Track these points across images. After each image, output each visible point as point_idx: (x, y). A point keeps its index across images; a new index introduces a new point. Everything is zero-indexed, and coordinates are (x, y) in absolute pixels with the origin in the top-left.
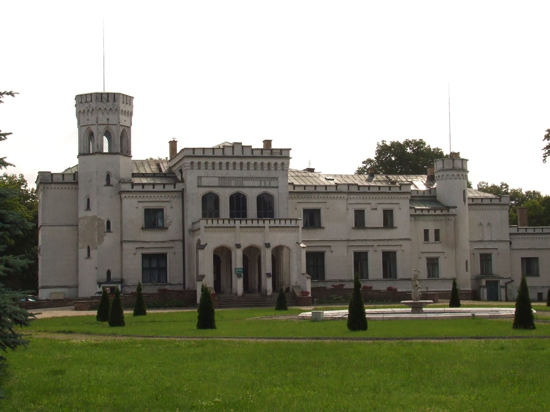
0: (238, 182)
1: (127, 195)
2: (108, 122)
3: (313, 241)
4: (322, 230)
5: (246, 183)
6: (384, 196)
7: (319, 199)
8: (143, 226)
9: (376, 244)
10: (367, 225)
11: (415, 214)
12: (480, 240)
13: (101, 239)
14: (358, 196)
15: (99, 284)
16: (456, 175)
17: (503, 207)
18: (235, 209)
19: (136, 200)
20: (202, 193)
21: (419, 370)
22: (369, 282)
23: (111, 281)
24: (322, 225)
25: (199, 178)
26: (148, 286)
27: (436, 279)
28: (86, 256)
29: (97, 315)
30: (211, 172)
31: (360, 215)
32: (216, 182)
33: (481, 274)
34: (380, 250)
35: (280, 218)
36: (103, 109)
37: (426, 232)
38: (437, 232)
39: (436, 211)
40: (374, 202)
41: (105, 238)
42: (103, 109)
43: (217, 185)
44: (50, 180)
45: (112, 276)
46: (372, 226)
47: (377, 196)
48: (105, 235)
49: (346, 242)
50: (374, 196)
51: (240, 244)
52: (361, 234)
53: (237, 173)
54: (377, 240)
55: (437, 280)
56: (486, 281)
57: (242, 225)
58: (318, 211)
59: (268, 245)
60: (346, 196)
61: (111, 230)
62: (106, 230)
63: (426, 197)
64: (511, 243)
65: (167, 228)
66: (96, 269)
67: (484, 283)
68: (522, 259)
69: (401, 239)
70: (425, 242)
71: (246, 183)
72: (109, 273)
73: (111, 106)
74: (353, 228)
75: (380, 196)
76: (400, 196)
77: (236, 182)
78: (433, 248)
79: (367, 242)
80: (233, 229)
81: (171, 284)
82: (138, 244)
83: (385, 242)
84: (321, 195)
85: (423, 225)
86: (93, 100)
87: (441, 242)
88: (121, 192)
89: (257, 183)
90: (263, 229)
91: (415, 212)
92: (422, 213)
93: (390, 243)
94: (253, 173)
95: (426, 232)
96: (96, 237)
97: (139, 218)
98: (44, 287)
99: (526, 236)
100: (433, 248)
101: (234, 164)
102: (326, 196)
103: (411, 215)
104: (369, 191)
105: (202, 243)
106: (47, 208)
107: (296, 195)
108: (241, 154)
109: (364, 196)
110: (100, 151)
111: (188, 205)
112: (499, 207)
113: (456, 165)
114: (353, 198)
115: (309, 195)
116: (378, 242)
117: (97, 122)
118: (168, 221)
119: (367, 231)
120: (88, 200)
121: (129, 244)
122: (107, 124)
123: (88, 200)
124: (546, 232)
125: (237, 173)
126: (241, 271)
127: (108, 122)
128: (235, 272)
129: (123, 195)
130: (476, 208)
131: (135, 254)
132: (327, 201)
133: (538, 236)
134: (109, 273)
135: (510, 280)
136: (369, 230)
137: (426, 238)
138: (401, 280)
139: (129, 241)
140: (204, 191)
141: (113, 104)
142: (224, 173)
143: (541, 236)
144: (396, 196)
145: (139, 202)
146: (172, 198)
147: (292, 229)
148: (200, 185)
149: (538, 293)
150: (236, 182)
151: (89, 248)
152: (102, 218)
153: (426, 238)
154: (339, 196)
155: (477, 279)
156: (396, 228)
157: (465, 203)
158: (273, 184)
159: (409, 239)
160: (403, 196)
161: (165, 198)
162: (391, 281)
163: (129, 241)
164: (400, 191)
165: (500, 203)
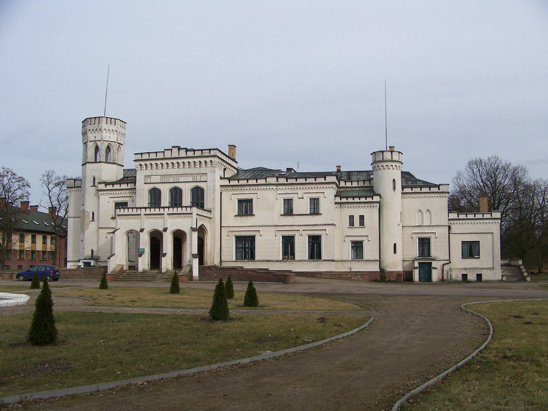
1: (102, 193)
2: (95, 139)
3: (245, 226)
4: (253, 217)
5: (182, 179)
6: (310, 186)
7: (265, 190)
8: (113, 216)
9: (301, 228)
11: (340, 201)
12: (419, 225)
14: (287, 187)
20: (191, 187)
21: (302, 358)
22: (295, 262)
24: (254, 214)
25: (146, 177)
27: (359, 261)
30: (154, 172)
31: (288, 203)
32: (157, 179)
33: (419, 257)
35: (137, 207)
36: (91, 129)
37: (351, 218)
38: (362, 218)
39: (361, 199)
40: (300, 193)
41: (90, 225)
42: (91, 129)
43: (159, 182)
44: (74, 184)
46: (299, 213)
47: (304, 187)
49: (274, 227)
50: (301, 187)
51: (166, 231)
52: (289, 220)
53: (171, 171)
54: (303, 225)
55: (361, 262)
58: (250, 201)
60: (274, 187)
61: (95, 220)
63: (366, 187)
64: (450, 228)
65: (254, 215)
68: (463, 242)
69: (325, 225)
70: (350, 227)
71: (182, 179)
72: (92, 251)
74: (281, 215)
75: (307, 186)
76: (325, 186)
79: (294, 227)
80: (139, 217)
82: (109, 229)
83: (311, 227)
84: (252, 187)
85: (348, 211)
87: (365, 227)
89: (190, 179)
91: (341, 200)
92: (347, 201)
93: (315, 228)
94: (187, 170)
95: (351, 218)
99: (467, 222)
100: (357, 233)
101: (173, 163)
102: (257, 188)
104: (297, 182)
108: (177, 156)
109: (292, 187)
113: (386, 157)
114: (282, 188)
116: (304, 227)
119: (294, 216)
122: (94, 140)
124: (487, 218)
125: (175, 171)
127: (95, 139)
130: (410, 196)
132: (258, 192)
133: (478, 221)
136: (295, 216)
138: (324, 261)
139: (102, 228)
141: (98, 125)
142: (165, 171)
143: (481, 221)
144: (321, 186)
145: (110, 197)
148: (146, 182)
149: (477, 274)
153: (352, 223)
154: (268, 187)
156: (254, 215)
157: (394, 191)
158: (203, 178)
159: (333, 225)
160: (328, 186)
162: (315, 262)
163: (102, 228)
164: (325, 181)
165: (439, 191)
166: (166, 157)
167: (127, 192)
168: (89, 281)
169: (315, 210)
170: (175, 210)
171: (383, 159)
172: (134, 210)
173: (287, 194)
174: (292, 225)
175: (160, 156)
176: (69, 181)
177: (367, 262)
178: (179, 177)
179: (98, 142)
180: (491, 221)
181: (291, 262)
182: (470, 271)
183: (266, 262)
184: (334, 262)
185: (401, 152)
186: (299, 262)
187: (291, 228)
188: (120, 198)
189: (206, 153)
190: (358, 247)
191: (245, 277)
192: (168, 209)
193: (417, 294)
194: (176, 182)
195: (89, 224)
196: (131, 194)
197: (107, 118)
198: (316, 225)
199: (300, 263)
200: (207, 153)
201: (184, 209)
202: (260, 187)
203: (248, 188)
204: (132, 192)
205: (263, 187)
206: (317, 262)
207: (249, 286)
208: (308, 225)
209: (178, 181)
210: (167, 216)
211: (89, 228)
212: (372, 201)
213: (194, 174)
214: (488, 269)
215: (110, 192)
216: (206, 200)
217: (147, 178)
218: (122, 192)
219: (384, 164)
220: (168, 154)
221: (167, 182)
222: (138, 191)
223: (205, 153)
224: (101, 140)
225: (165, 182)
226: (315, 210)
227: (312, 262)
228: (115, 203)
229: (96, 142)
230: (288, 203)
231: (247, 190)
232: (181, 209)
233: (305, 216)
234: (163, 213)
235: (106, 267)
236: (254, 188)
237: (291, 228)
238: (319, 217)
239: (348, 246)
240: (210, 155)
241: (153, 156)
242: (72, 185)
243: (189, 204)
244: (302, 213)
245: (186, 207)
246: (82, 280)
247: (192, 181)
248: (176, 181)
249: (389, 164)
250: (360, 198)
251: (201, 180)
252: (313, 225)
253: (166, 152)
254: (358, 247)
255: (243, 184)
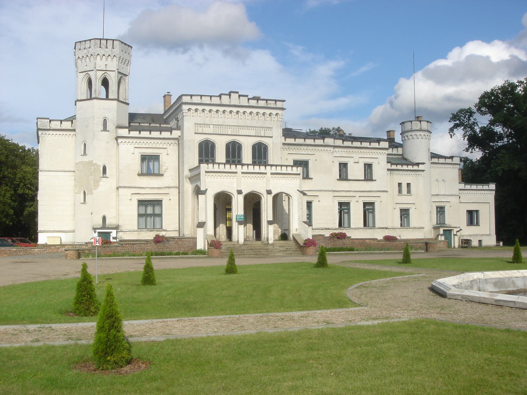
0: (234, 131)
1: (123, 140)
5: (242, 132)
6: (365, 150)
9: (357, 194)
10: (349, 178)
13: (97, 184)
15: (95, 229)
16: (422, 135)
17: (454, 166)
18: (231, 157)
19: (133, 146)
20: (198, 140)
22: (352, 230)
23: (107, 226)
26: (144, 232)
28: (82, 201)
29: (502, 39)
31: (343, 166)
34: (361, 201)
37: (400, 185)
38: (409, 185)
41: (101, 183)
45: (107, 222)
46: (354, 178)
48: (101, 180)
50: (357, 150)
52: (344, 185)
56: (444, 230)
57: (243, 171)
59: (269, 192)
60: (332, 149)
62: (102, 176)
66: (92, 214)
67: (441, 232)
72: (104, 218)
73: (110, 53)
74: (338, 180)
75: (362, 150)
76: (379, 151)
77: (232, 131)
78: (405, 200)
79: (372, 193)
81: (165, 231)
82: (134, 189)
86: (92, 47)
88: (117, 138)
89: (253, 133)
90: (265, 175)
91: (391, 167)
93: (370, 194)
95: (400, 185)
96: (92, 182)
97: (136, 164)
98: (275, 208)
100: (405, 200)
102: (314, 148)
103: (388, 170)
105: (202, 189)
106: (45, 154)
107: (287, 147)
109: (348, 150)
110: (97, 96)
111: (186, 152)
112: (451, 166)
115: (299, 147)
116: (359, 193)
117: (95, 68)
118: (164, 168)
120: (85, 144)
121: (125, 189)
123: (85, 144)
126: (243, 218)
128: (236, 218)
129: (120, 140)
131: (130, 200)
134: (104, 218)
135: (459, 230)
136: (351, 182)
137: (400, 191)
138: (379, 228)
139: (124, 187)
140: (202, 138)
145: (135, 147)
146: (168, 145)
147: (293, 176)
148: (197, 132)
150: (232, 131)
151: (85, 193)
152: (98, 163)
153: (400, 191)
155: (436, 228)
159: (386, 191)
161: (161, 144)
163: (124, 187)
166: (224, 103)
167: (145, 142)
168: (106, 259)
169: (368, 176)
170: (257, 169)
171: (421, 128)
172: (288, 168)
173: (343, 158)
174: (349, 191)
175: (216, 100)
176: (42, 120)
177: (414, 229)
178: (240, 129)
179: (110, 72)
180: (488, 192)
181: (348, 230)
182: (474, 237)
183: (324, 230)
184: (387, 230)
185: (430, 121)
186: (356, 230)
187: (347, 194)
188: (149, 149)
189: (272, 104)
190: (405, 213)
191: (362, 247)
192: (280, 167)
193: (161, 260)
194: (233, 135)
195: (100, 181)
196: (165, 145)
197: (107, 40)
198: (371, 191)
199: (356, 231)
200: (272, 104)
201: (216, 166)
202: (317, 148)
203: (305, 148)
204: (166, 143)
205: (320, 148)
206: (372, 230)
207: (404, 256)
208: (363, 191)
209: (237, 134)
210: (270, 176)
211: (100, 187)
212: (418, 169)
213: (257, 127)
214: (486, 235)
215: (135, 141)
216: (272, 158)
217: (198, 127)
218: (152, 141)
219: (413, 133)
220: (225, 100)
221: (224, 133)
222: (186, 142)
223: (270, 104)
224: (93, 70)
225: (222, 133)
226: (368, 176)
227: (367, 230)
228: (141, 155)
229: (88, 72)
230: (343, 166)
231: (303, 150)
232: (212, 165)
233: (360, 182)
234: (235, 171)
235: (194, 239)
236: (311, 148)
237: (347, 194)
238: (374, 183)
239: (397, 214)
240: (276, 106)
241: (206, 100)
242: (46, 127)
243: (250, 161)
244: (357, 179)
245: (219, 164)
246: (448, 256)
247: (255, 135)
248: (235, 134)
249: (418, 133)
250: (397, 164)
251: (266, 135)
252: (368, 191)
253: (223, 97)
254: (405, 213)
255: (300, 143)
